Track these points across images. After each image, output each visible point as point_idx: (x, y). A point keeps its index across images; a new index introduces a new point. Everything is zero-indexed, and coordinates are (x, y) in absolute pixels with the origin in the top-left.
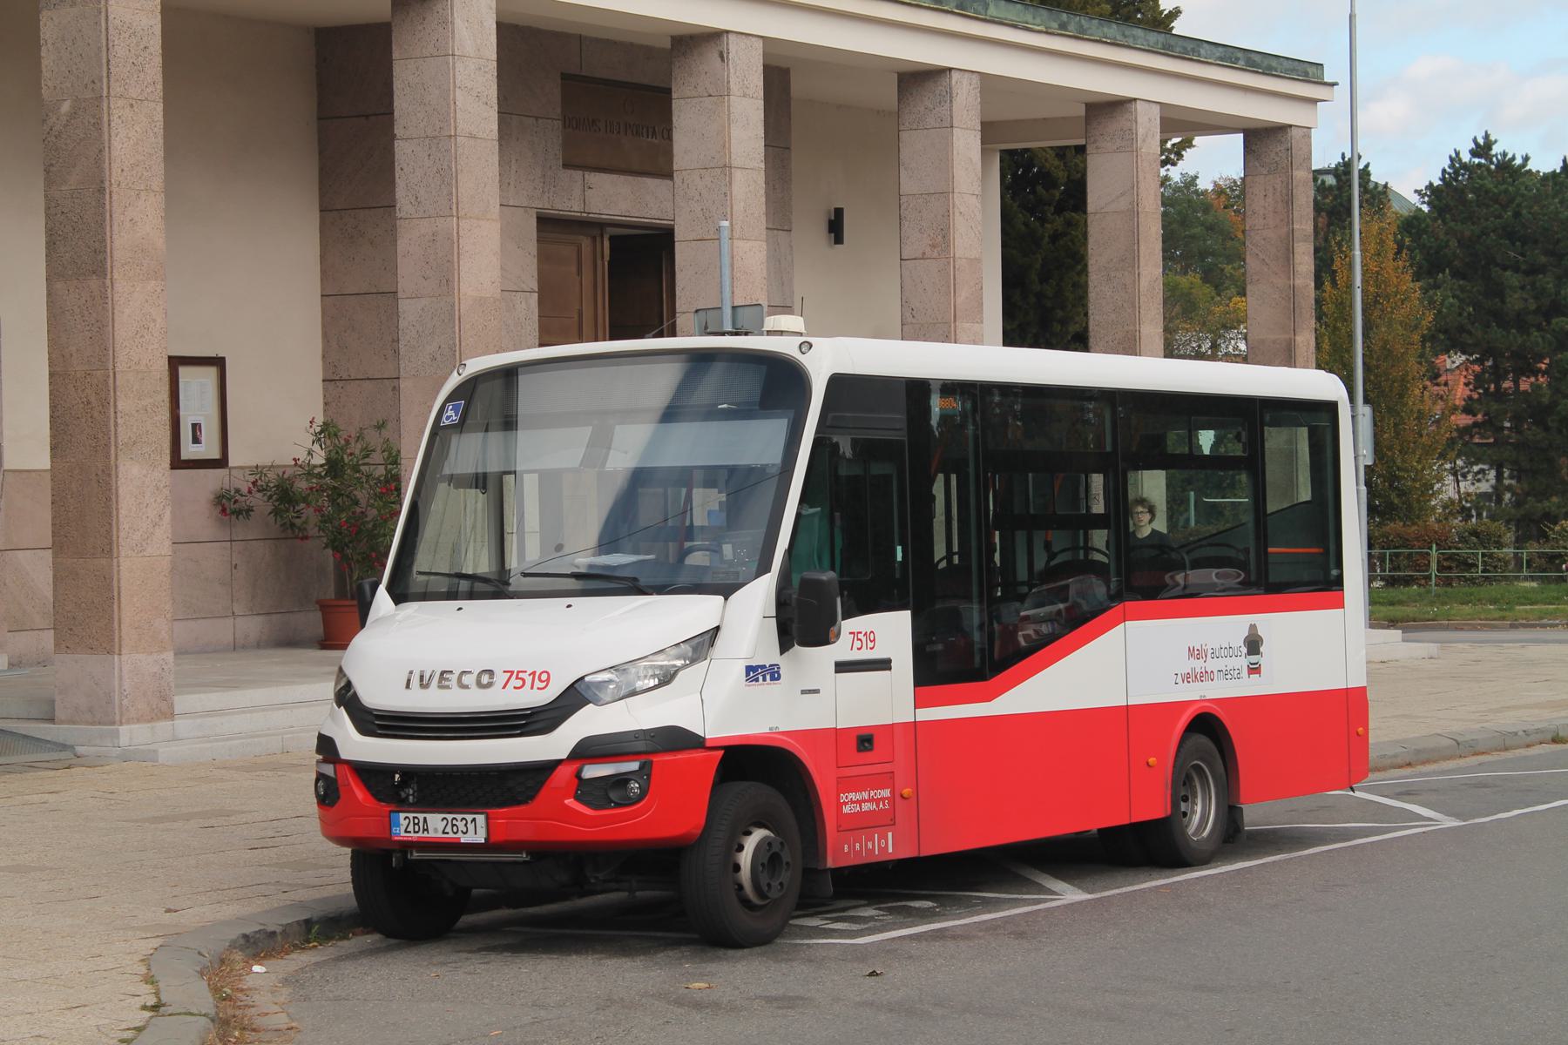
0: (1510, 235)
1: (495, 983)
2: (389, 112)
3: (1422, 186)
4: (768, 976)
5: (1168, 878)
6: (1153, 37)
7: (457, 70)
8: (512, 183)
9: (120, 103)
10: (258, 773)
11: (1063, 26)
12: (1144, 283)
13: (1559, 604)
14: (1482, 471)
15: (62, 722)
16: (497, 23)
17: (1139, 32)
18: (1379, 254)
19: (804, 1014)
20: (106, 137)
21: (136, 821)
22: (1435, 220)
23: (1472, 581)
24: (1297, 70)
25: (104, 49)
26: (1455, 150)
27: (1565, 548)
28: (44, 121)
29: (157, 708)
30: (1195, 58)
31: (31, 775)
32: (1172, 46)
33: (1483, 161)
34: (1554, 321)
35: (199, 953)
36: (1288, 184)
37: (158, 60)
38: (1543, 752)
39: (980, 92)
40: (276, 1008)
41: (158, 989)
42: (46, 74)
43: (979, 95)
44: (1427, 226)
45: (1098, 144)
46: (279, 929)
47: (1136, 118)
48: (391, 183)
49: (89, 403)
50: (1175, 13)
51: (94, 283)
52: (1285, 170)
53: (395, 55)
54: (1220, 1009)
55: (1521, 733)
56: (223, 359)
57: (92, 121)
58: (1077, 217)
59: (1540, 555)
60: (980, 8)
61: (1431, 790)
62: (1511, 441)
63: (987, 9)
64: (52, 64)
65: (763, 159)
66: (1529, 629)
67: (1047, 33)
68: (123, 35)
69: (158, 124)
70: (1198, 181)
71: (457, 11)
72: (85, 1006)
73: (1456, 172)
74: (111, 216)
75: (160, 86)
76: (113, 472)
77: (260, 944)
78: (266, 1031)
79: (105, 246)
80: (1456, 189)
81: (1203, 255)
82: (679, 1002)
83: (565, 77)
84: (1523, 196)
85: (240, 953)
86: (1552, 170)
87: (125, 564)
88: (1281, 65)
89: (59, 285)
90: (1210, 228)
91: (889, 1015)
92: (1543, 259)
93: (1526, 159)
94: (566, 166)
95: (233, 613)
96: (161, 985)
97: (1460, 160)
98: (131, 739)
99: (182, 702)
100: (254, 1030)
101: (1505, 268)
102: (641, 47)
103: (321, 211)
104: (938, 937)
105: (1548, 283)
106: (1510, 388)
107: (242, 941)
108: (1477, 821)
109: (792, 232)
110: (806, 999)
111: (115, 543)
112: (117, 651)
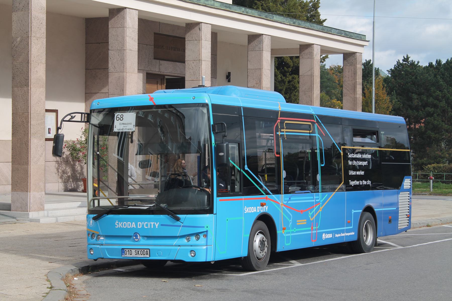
1: (142, 284)
2: (107, 42)
3: (389, 69)
4: (217, 283)
5: (323, 260)
6: (319, 27)
7: (127, 31)
8: (139, 63)
9: (34, 38)
10: (68, 226)
13: (427, 189)
15: (13, 211)
16: (138, 18)
17: (315, 25)
18: (378, 89)
19: (228, 293)
20: (30, 48)
21: (36, 238)
22: (392, 79)
24: (359, 37)
25: (30, 23)
26: (398, 60)
28: (13, 43)
29: (40, 207)
30: (330, 33)
31: (5, 225)
32: (324, 29)
33: (406, 63)
34: (426, 108)
35: (60, 274)
36: (355, 69)
37: (45, 27)
38: (424, 229)
39: (271, 41)
40: (82, 289)
41: (51, 283)
42: (13, 30)
43: (270, 41)
44: (391, 81)
45: (303, 56)
47: (314, 49)
48: (107, 62)
49: (23, 122)
50: (324, 21)
51: (25, 88)
52: (354, 64)
53: (110, 27)
54: (341, 294)
55: (418, 224)
56: (57, 110)
57: (26, 43)
58: (296, 76)
59: (422, 175)
60: (271, 18)
61: (394, 238)
62: (413, 142)
63: (273, 18)
64: (15, 27)
65: (210, 58)
66: (418, 195)
68: (35, 20)
69: (44, 45)
70: (325, 66)
71: (127, 15)
72: (32, 287)
73: (399, 66)
74: (31, 70)
75: (45, 34)
76: (29, 141)
77: (75, 272)
78: (81, 295)
79: (29, 78)
80: (399, 71)
81: (326, 87)
82: (193, 290)
83: (155, 34)
84: (418, 73)
85: (70, 274)
86: (426, 66)
87: (32, 167)
88: (354, 35)
89: (16, 89)
90: (329, 80)
91: (251, 294)
92: (423, 91)
93: (418, 62)
94: (155, 59)
95: (58, 182)
96: (52, 282)
97: (400, 62)
98: (32, 216)
99: (47, 206)
100: (77, 295)
101: (413, 93)
102: (176, 26)
103: (86, 69)
104: (262, 274)
105: (425, 98)
106: (413, 127)
107: (71, 271)
108: (407, 247)
109: (217, 79)
110: (228, 290)
111: (29, 161)
112: (29, 191)
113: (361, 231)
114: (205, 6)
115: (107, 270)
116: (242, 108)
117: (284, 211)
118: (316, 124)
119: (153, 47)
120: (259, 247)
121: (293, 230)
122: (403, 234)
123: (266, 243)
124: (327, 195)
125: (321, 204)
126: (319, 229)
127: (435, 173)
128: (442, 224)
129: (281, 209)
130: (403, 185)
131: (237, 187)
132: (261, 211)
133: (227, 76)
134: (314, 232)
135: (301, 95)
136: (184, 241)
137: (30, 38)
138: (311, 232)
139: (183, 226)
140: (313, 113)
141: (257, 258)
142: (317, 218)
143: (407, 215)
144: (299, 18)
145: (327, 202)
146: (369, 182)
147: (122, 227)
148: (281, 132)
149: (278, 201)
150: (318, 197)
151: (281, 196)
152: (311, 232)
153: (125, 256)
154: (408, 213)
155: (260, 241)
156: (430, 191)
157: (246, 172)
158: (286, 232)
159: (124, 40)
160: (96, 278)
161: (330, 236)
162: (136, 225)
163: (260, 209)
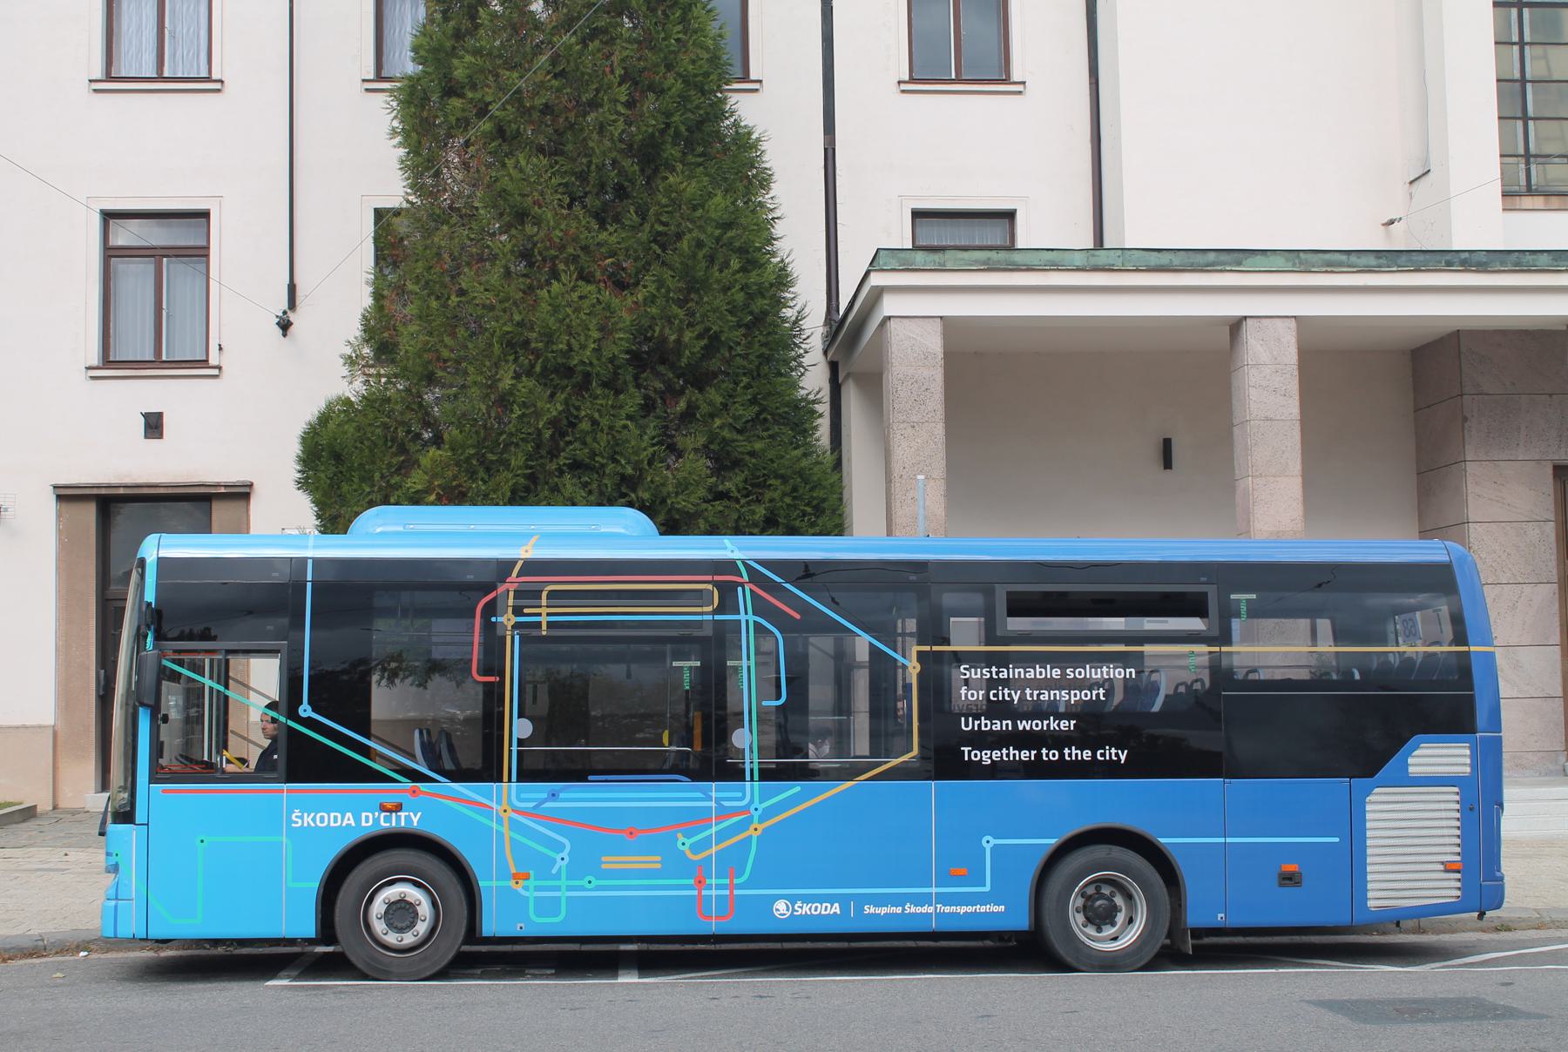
117: (513, 825)
125: (756, 815)
126: (741, 887)
132: (380, 824)
147: (313, 825)
150: (740, 794)
158: (535, 887)
162: (357, 819)
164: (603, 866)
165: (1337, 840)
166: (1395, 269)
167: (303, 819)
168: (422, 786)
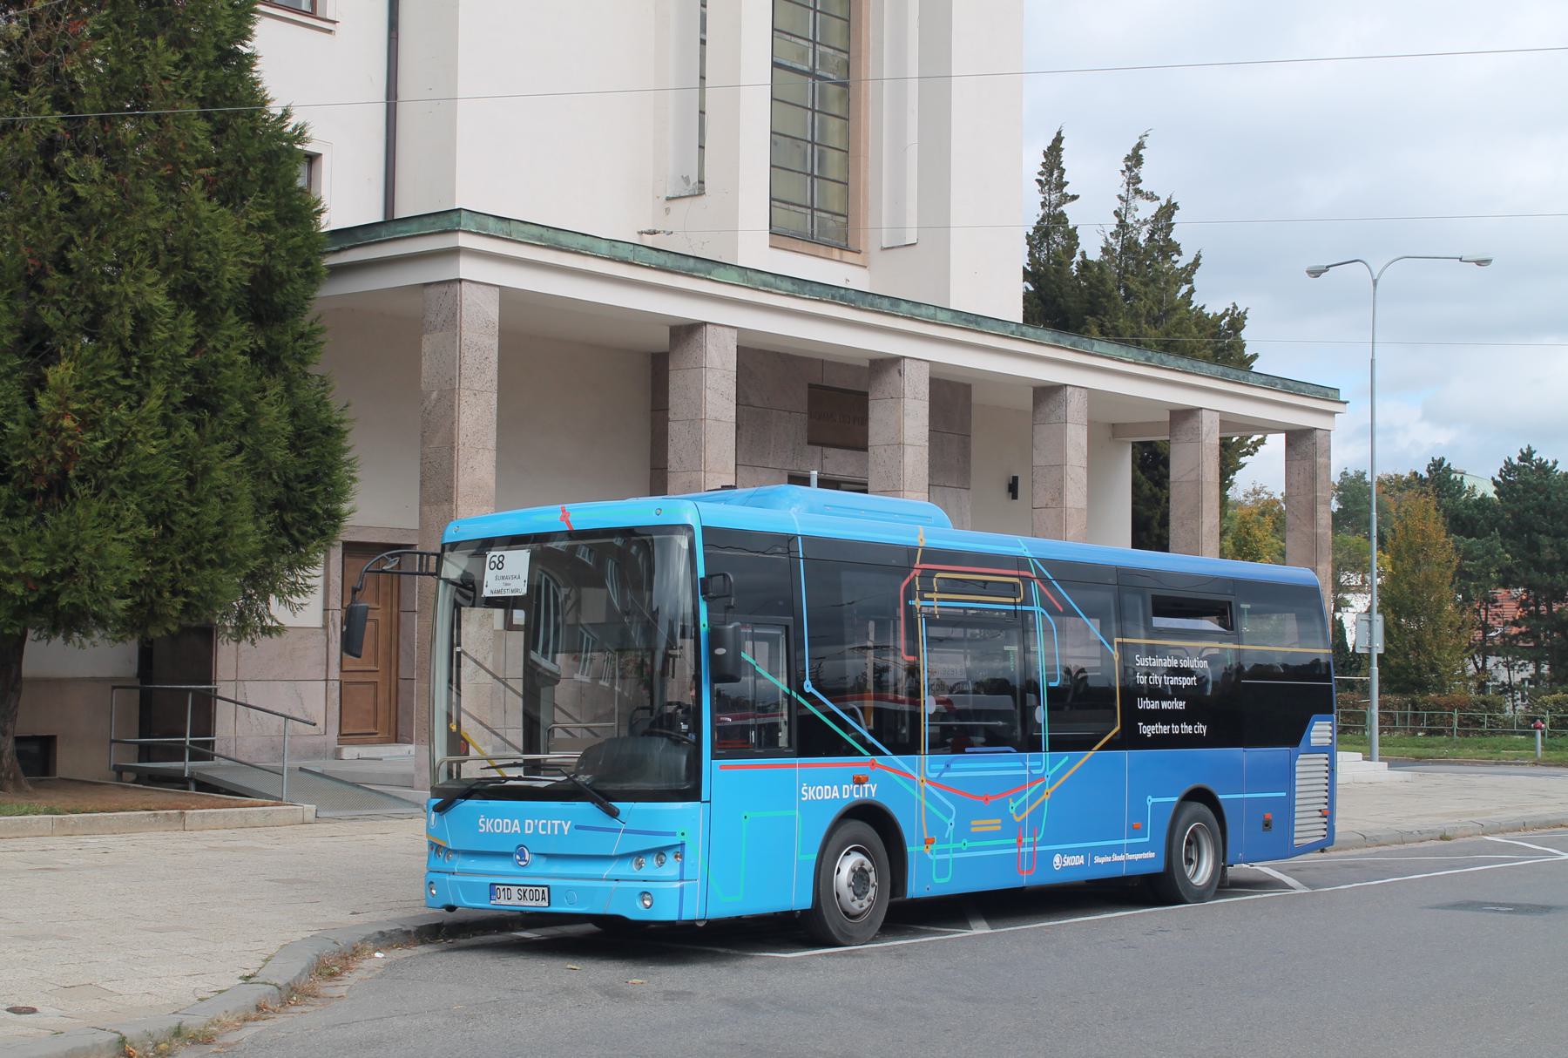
0: (1542, 510)
9: (467, 392)
11: (1148, 359)
12: (1205, 528)
14: (1524, 664)
17: (1204, 365)
23: (1482, 734)
27: (1565, 713)
42: (424, 374)
46: (413, 929)
50: (1255, 357)
51: (446, 507)
53: (671, 367)
67: (1135, 363)
75: (495, 383)
83: (811, 386)
89: (426, 508)
93: (1556, 463)
94: (809, 443)
107: (378, 936)
113: (1174, 851)
114: (911, 319)
115: (497, 934)
116: (799, 538)
117: (928, 795)
118: (1036, 581)
119: (805, 416)
120: (849, 885)
121: (960, 845)
122: (1314, 857)
123: (872, 876)
124: (1067, 758)
125: (1047, 780)
126: (1042, 843)
127: (1559, 716)
128: (1483, 834)
129: (920, 793)
130: (1310, 738)
131: (783, 737)
133: (1010, 485)
134: (1025, 850)
135: (1175, 531)
136: (627, 869)
137: (457, 391)
138: (1016, 850)
139: (625, 831)
140: (1028, 554)
141: (846, 913)
142: (1036, 815)
143: (1320, 811)
144: (1192, 352)
145: (1063, 779)
146: (1201, 729)
148: (922, 599)
149: (911, 772)
150: (1039, 763)
151: (920, 759)
152: (1016, 850)
153: (498, 901)
154: (1326, 807)
155: (853, 870)
156: (1536, 755)
157: (809, 697)
159: (700, 395)
160: (444, 955)
161: (1079, 860)
163: (851, 791)
164: (973, 829)
165: (1284, 794)
166: (807, 296)
167: (809, 793)
168: (878, 759)
